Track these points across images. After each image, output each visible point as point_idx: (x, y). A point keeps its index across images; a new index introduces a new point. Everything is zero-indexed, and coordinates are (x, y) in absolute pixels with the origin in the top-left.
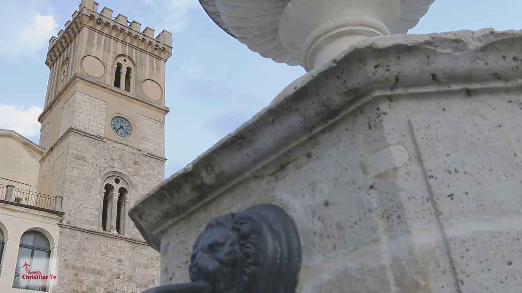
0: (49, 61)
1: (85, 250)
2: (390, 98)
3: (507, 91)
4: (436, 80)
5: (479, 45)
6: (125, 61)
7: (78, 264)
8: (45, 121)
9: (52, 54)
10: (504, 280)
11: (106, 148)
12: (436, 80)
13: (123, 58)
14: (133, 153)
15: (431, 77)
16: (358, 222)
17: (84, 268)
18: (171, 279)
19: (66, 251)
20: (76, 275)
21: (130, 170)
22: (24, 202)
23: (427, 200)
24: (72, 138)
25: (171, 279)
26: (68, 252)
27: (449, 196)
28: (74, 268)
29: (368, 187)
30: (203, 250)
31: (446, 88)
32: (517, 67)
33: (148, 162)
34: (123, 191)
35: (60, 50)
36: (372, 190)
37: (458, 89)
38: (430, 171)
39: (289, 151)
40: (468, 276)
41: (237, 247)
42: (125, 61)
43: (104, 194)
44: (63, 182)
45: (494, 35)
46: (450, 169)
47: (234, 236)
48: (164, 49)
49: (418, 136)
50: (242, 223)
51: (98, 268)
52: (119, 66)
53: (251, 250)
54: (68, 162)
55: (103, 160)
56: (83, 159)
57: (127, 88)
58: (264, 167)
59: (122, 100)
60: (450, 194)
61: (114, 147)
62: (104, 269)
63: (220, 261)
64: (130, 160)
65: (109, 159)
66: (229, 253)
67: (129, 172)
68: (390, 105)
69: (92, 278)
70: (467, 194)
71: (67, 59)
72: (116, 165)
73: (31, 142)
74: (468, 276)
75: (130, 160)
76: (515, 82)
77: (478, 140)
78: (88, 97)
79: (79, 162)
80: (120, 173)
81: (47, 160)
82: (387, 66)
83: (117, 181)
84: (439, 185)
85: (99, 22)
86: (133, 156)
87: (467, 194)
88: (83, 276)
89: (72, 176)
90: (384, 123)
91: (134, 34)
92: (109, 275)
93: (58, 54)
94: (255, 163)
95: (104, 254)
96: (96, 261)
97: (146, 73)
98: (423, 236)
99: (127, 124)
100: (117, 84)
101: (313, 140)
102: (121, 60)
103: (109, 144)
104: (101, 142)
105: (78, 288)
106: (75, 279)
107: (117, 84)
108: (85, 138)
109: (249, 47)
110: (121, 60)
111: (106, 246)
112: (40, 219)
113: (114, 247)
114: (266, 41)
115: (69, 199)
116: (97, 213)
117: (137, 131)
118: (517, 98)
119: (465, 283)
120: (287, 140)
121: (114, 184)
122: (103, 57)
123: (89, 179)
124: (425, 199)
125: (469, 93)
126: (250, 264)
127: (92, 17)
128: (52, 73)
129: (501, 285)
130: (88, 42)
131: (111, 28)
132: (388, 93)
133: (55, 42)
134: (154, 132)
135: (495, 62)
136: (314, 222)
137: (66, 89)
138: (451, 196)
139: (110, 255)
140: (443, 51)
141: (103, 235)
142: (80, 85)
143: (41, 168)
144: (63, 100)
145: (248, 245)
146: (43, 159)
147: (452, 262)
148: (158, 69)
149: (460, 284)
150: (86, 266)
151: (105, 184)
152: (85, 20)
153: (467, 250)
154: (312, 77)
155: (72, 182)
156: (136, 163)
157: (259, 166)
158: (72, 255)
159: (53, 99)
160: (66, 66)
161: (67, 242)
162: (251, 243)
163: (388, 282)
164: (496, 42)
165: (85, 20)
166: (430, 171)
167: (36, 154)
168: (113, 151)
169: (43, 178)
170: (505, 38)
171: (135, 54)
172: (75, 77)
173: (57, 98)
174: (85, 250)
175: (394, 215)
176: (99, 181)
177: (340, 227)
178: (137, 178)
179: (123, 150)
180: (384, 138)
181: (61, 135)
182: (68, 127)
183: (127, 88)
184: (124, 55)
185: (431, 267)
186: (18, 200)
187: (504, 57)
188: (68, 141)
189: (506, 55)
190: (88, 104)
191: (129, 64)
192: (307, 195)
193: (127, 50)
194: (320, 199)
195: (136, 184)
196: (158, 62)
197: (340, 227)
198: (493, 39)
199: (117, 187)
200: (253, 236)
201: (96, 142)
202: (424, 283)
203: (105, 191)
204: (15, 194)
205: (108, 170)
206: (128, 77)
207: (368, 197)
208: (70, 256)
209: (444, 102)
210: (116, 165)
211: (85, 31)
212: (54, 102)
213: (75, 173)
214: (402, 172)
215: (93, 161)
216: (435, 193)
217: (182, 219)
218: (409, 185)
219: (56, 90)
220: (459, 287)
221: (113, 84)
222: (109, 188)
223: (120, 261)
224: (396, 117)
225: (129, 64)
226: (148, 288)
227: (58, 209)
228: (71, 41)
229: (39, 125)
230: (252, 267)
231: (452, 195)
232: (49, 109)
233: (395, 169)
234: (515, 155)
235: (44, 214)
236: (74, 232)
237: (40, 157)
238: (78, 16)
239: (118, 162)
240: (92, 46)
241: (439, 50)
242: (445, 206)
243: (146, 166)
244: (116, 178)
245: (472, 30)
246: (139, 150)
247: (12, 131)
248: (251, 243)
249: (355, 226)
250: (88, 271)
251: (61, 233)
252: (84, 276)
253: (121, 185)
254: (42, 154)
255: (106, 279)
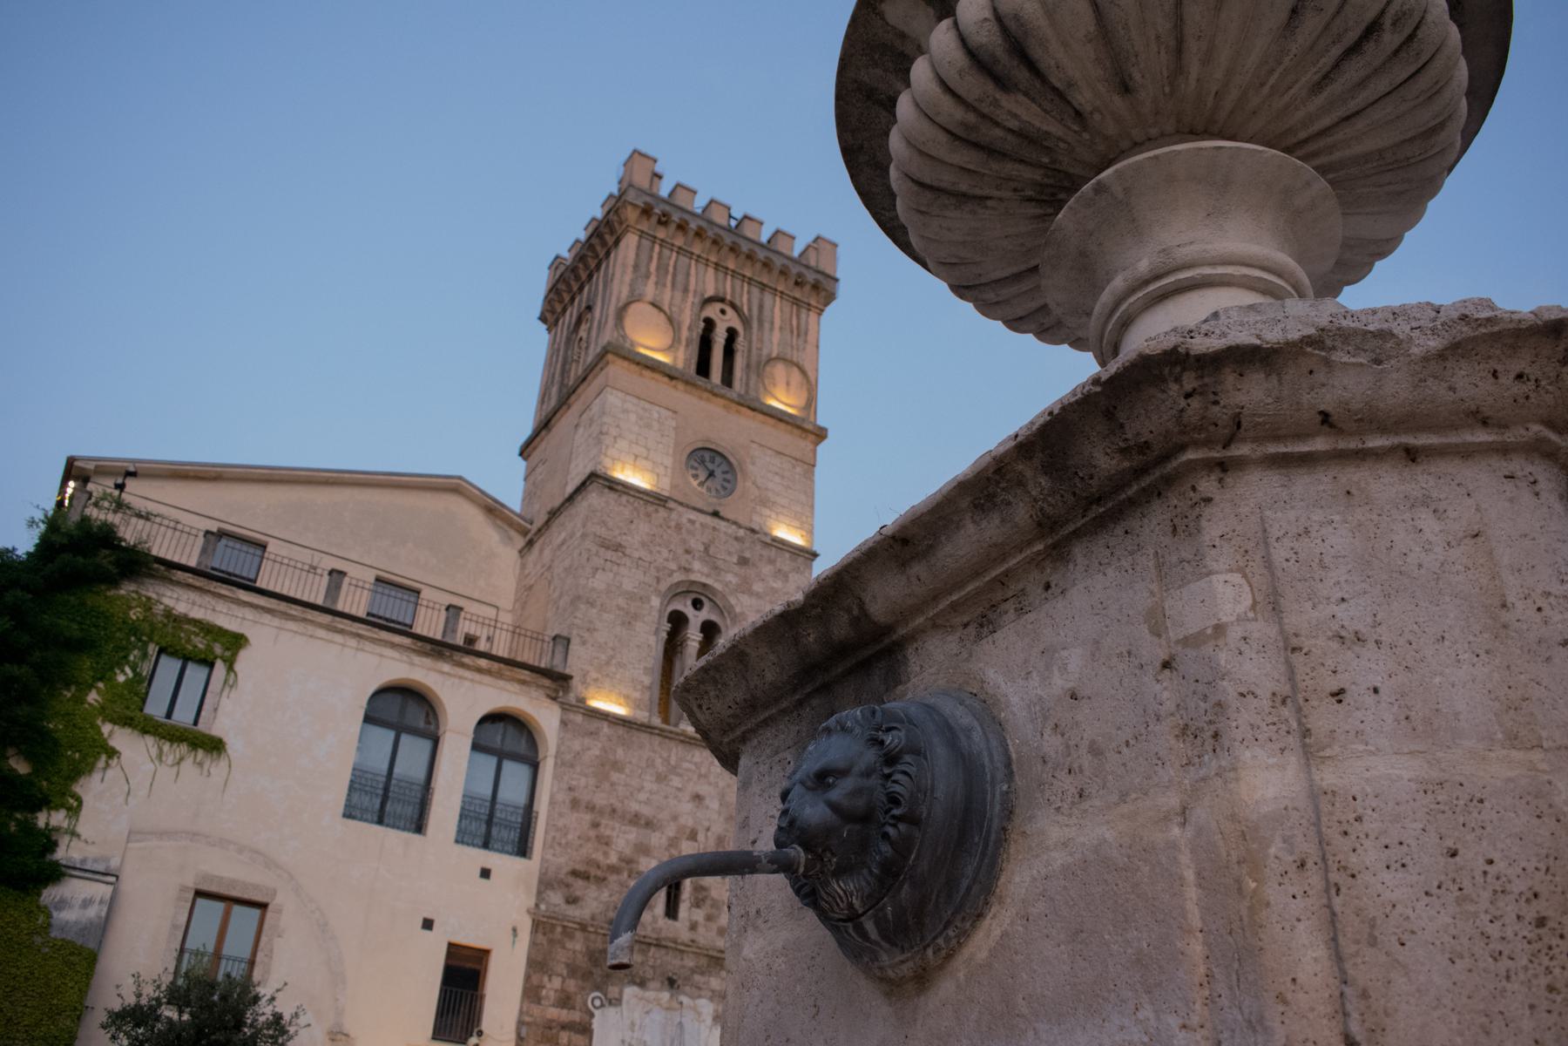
0: (548, 315)
1: (617, 766)
2: (1223, 466)
3: (1504, 450)
4: (1332, 426)
5: (1434, 344)
6: (723, 312)
7: (600, 800)
8: (536, 456)
9: (562, 286)
10: (1434, 891)
11: (673, 524)
12: (1332, 426)
13: (719, 306)
14: (737, 539)
15: (1319, 418)
16: (1132, 742)
17: (614, 811)
18: (754, 842)
19: (572, 766)
20: (596, 825)
21: (730, 577)
22: (482, 646)
23: (1284, 702)
24: (594, 499)
25: (754, 842)
26: (578, 769)
27: (1333, 695)
28: (591, 808)
29: (1158, 665)
30: (802, 783)
31: (1353, 444)
32: (1527, 398)
33: (771, 562)
34: (710, 630)
35: (573, 288)
36: (1167, 672)
37: (1381, 447)
38: (1296, 635)
39: (1006, 574)
40: (1353, 876)
41: (874, 781)
42: (723, 312)
43: (664, 635)
44: (572, 602)
45: (1468, 324)
46: (1343, 633)
47: (871, 756)
48: (816, 287)
49: (1280, 553)
50: (889, 729)
51: (646, 811)
52: (709, 324)
53: (901, 787)
54: (585, 556)
55: (665, 554)
56: (618, 547)
57: (728, 380)
58: (954, 607)
59: (715, 408)
60: (1335, 689)
61: (692, 522)
62: (660, 816)
63: (834, 807)
64: (730, 553)
65: (680, 551)
66: (857, 792)
67: (727, 584)
68: (1220, 480)
69: (633, 834)
70: (1376, 691)
71: (589, 308)
72: (697, 565)
73: (502, 505)
74: (1353, 876)
75: (730, 553)
76: (1523, 432)
77: (1420, 566)
78: (635, 401)
79: (609, 554)
80: (704, 585)
81: (537, 546)
82: (1215, 393)
83: (697, 604)
84: (1313, 669)
85: (664, 221)
86: (737, 545)
87: (1376, 691)
88: (610, 828)
89: (593, 589)
90: (1204, 523)
91: (745, 247)
92: (671, 831)
93: (567, 298)
94: (935, 598)
95: (661, 779)
96: (642, 796)
97: (774, 341)
98: (1266, 780)
99: (724, 467)
100: (703, 368)
101: (1059, 553)
102: (712, 311)
103: (680, 515)
104: (661, 510)
105: (599, 857)
106: (592, 833)
107: (703, 368)
108: (624, 498)
109: (977, 307)
110: (712, 311)
111: (667, 760)
112: (516, 687)
113: (686, 765)
114: (1012, 291)
115: (584, 643)
116: (647, 680)
117: (749, 484)
118: (1530, 468)
119: (1343, 890)
120: (999, 553)
121: (689, 611)
122: (671, 305)
123: (631, 597)
124: (1278, 700)
125: (1411, 455)
126: (899, 819)
127: (646, 212)
128: (553, 342)
129: (1427, 900)
130: (636, 267)
131: (691, 234)
132: (1216, 454)
133: (562, 268)
134: (788, 487)
135: (1470, 383)
136: (1046, 736)
137: (584, 379)
138: (1338, 695)
139: (676, 781)
140: (1345, 359)
141: (662, 734)
142: (616, 370)
143: (523, 567)
144: (576, 406)
145: (898, 777)
146: (530, 543)
147: (1322, 842)
148: (801, 333)
149: (1333, 891)
150: (618, 805)
151: (670, 609)
152: (631, 215)
153: (1359, 819)
154: (1051, 413)
155: (592, 604)
156: (743, 561)
157: (944, 604)
158: (586, 776)
159: (553, 402)
160: (584, 327)
161: (576, 745)
162: (905, 773)
163: (1182, 878)
164: (1474, 339)
165: (631, 215)
166: (1296, 635)
167: (513, 533)
168: (689, 532)
169: (526, 590)
170: (1496, 329)
171: (746, 297)
172: (605, 351)
173: (564, 402)
174: (617, 766)
175: (1206, 733)
176: (656, 602)
177: (1095, 750)
178: (746, 600)
179: (714, 529)
180: (1199, 557)
181: (570, 489)
182: (588, 471)
183: (728, 380)
184: (722, 300)
185: (1272, 851)
186: (471, 640)
187: (1495, 374)
188: (585, 504)
189: (1499, 368)
190: (633, 417)
191: (732, 319)
192: (1034, 674)
193: (728, 287)
194: (1059, 683)
195: (742, 613)
196: (803, 316)
197: (1095, 750)
198: (1467, 331)
199: (696, 618)
200: (908, 758)
201: (651, 508)
202: (1253, 885)
203: (667, 627)
204: (465, 627)
205: (678, 577)
206: (729, 352)
207: (1158, 687)
208: (583, 781)
209: (1353, 475)
210: (697, 565)
211: (630, 242)
212: (555, 412)
213: (599, 582)
214: (1235, 634)
215: (643, 553)
216: (1302, 685)
217: (783, 712)
218: (1254, 669)
219: (562, 384)
220: (1329, 899)
221: (693, 367)
222: (678, 621)
223: (698, 798)
224: (1251, 504)
225: (732, 319)
226: (675, 853)
227: (560, 669)
228: (598, 267)
229: (521, 465)
230: (902, 827)
231: (1342, 691)
232: (544, 426)
233: (1220, 629)
234: (1504, 606)
235: (525, 675)
236: (595, 724)
237: (520, 542)
238: (616, 205)
239: (700, 559)
240: (647, 276)
241: (1340, 357)
242: (1323, 717)
243: (767, 570)
244: (694, 596)
245: (1437, 302)
246: (753, 531)
247: (460, 478)
248: (905, 773)
249: (1125, 750)
250: (623, 817)
251: (564, 723)
252: (613, 829)
253: (705, 614)
254: (525, 533)
255: (664, 841)
